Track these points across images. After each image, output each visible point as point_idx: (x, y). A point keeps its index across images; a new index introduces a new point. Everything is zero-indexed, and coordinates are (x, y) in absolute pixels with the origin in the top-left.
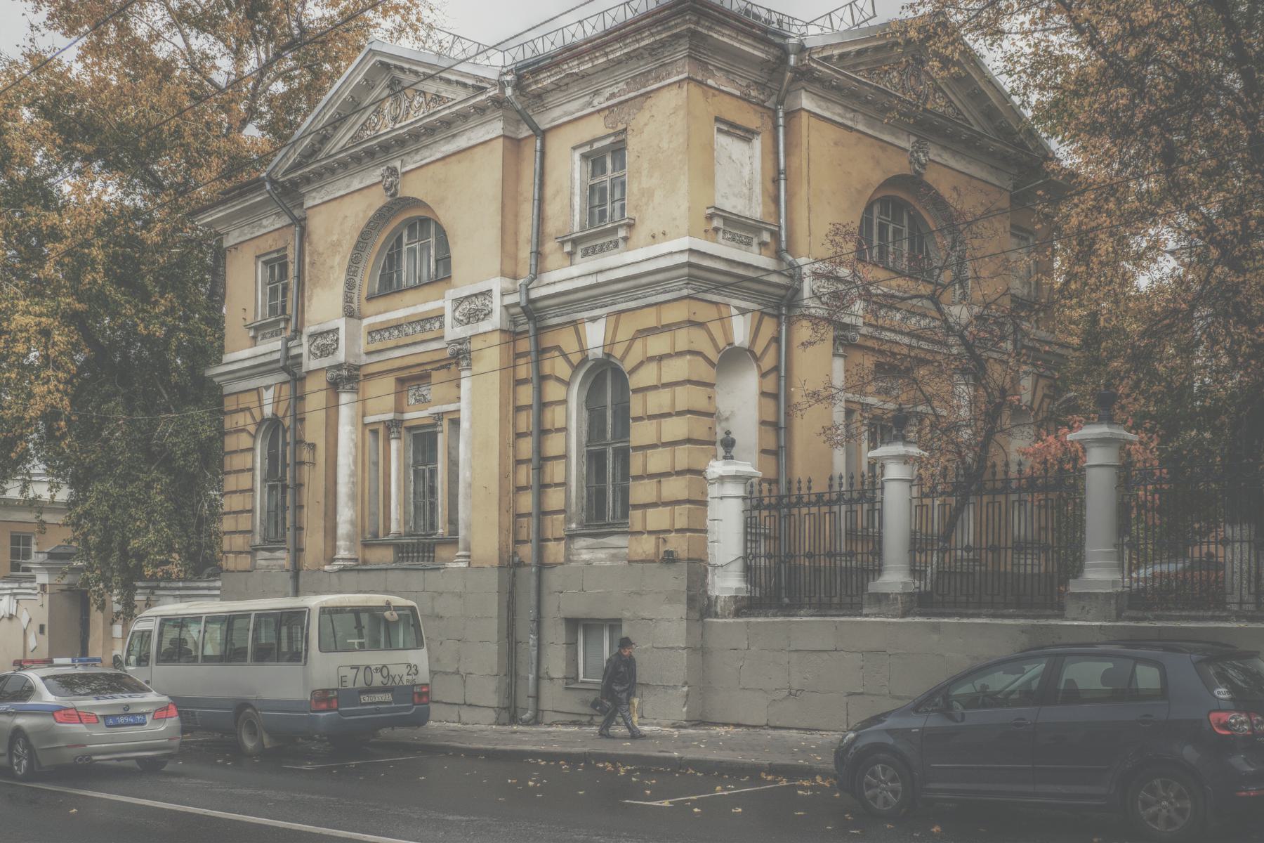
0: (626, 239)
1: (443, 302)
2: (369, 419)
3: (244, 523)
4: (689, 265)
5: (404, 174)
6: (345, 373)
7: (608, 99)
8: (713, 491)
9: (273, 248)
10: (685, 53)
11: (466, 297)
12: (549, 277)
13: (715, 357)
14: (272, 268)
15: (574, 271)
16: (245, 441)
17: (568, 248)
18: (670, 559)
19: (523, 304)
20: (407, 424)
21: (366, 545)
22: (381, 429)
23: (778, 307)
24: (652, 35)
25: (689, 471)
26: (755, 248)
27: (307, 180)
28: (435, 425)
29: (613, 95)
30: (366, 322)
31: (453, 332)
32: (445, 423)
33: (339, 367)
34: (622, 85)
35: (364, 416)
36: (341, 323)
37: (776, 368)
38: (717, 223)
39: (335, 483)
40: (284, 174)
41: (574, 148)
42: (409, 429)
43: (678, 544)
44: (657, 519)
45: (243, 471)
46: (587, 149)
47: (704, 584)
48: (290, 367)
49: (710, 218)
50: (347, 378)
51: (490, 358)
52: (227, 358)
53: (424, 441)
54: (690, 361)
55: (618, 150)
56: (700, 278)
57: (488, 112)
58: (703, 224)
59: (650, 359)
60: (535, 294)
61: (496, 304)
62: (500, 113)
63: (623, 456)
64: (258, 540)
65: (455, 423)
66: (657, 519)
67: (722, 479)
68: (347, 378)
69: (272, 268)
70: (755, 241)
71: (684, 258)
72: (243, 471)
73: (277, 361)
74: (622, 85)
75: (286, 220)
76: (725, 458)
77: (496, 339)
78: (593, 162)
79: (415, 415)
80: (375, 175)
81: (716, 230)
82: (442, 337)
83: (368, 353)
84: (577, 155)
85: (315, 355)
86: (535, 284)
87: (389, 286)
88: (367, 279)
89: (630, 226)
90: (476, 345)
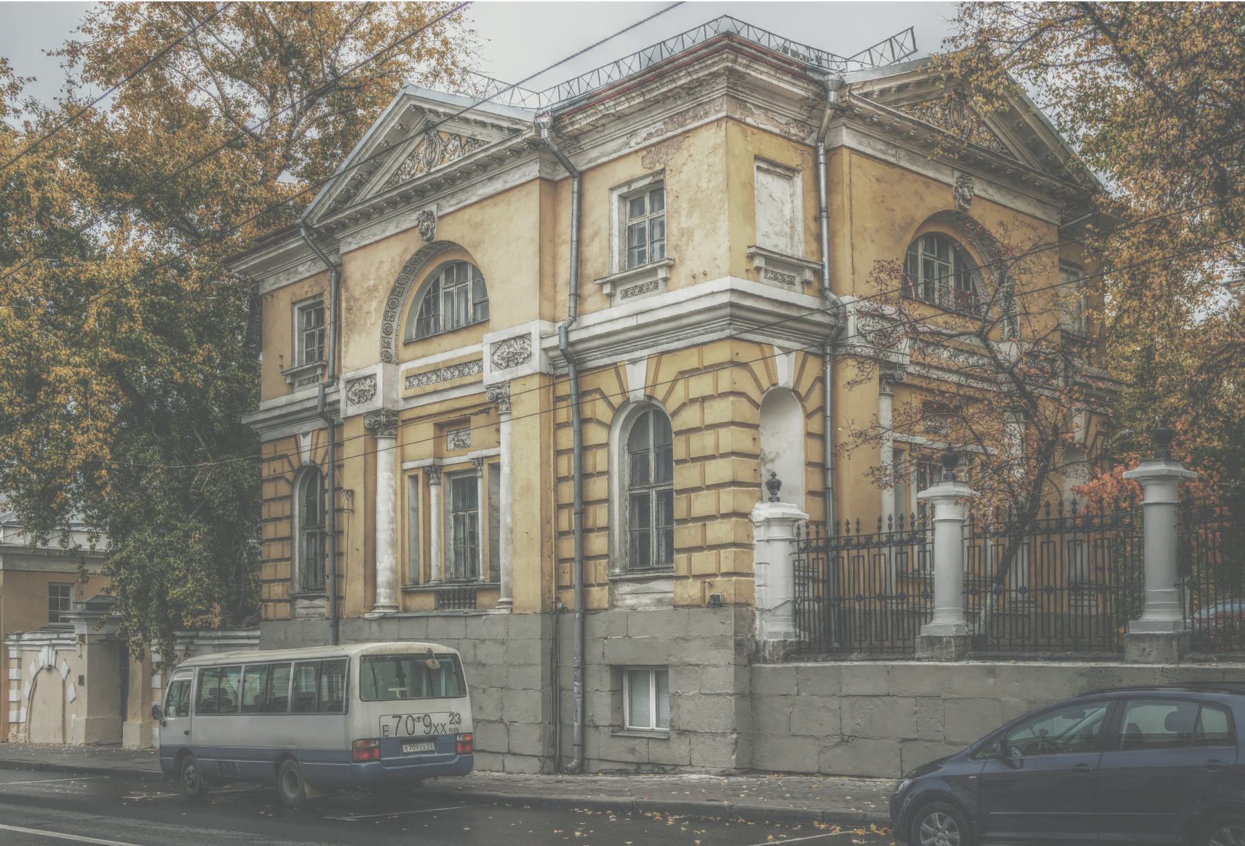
0: (666, 280)
1: (481, 345)
2: (408, 465)
3: (283, 570)
4: (732, 305)
5: (440, 218)
6: (383, 419)
7: (645, 139)
8: (759, 534)
9: (309, 295)
10: (724, 91)
11: (504, 341)
12: (587, 320)
13: (758, 398)
14: (309, 315)
15: (615, 312)
16: (283, 488)
17: (607, 289)
18: (716, 603)
19: (563, 347)
20: (446, 470)
21: (407, 592)
22: (420, 474)
23: (823, 346)
24: (689, 74)
25: (735, 514)
26: (798, 287)
27: (342, 226)
28: (475, 470)
29: (650, 135)
30: (403, 367)
31: (492, 376)
32: (485, 468)
33: (376, 413)
34: (659, 125)
35: (403, 462)
36: (379, 370)
37: (822, 409)
38: (759, 262)
39: (375, 530)
40: (318, 222)
41: (612, 189)
42: (449, 474)
43: (724, 588)
44: (703, 562)
45: (280, 519)
46: (625, 190)
47: (751, 629)
48: (328, 415)
49: (751, 257)
50: (386, 424)
51: (529, 402)
52: (263, 405)
53: (463, 487)
54: (733, 403)
55: (657, 190)
56: (742, 318)
57: (524, 154)
58: (744, 264)
59: (693, 401)
60: (574, 337)
61: (535, 346)
62: (536, 155)
63: (667, 499)
64: (297, 588)
65: (496, 468)
66: (703, 562)
67: (768, 522)
68: (386, 424)
69: (309, 315)
70: (798, 280)
71: (726, 298)
72: (280, 519)
73: (315, 408)
74: (659, 125)
75: (322, 266)
76: (771, 500)
77: (535, 383)
78: (631, 202)
79: (456, 459)
80: (409, 221)
81: (758, 269)
82: (481, 382)
83: (406, 399)
84: (615, 197)
85: (352, 401)
86: (574, 326)
87: (426, 330)
88: (404, 325)
89: (670, 267)
90: (515, 389)
